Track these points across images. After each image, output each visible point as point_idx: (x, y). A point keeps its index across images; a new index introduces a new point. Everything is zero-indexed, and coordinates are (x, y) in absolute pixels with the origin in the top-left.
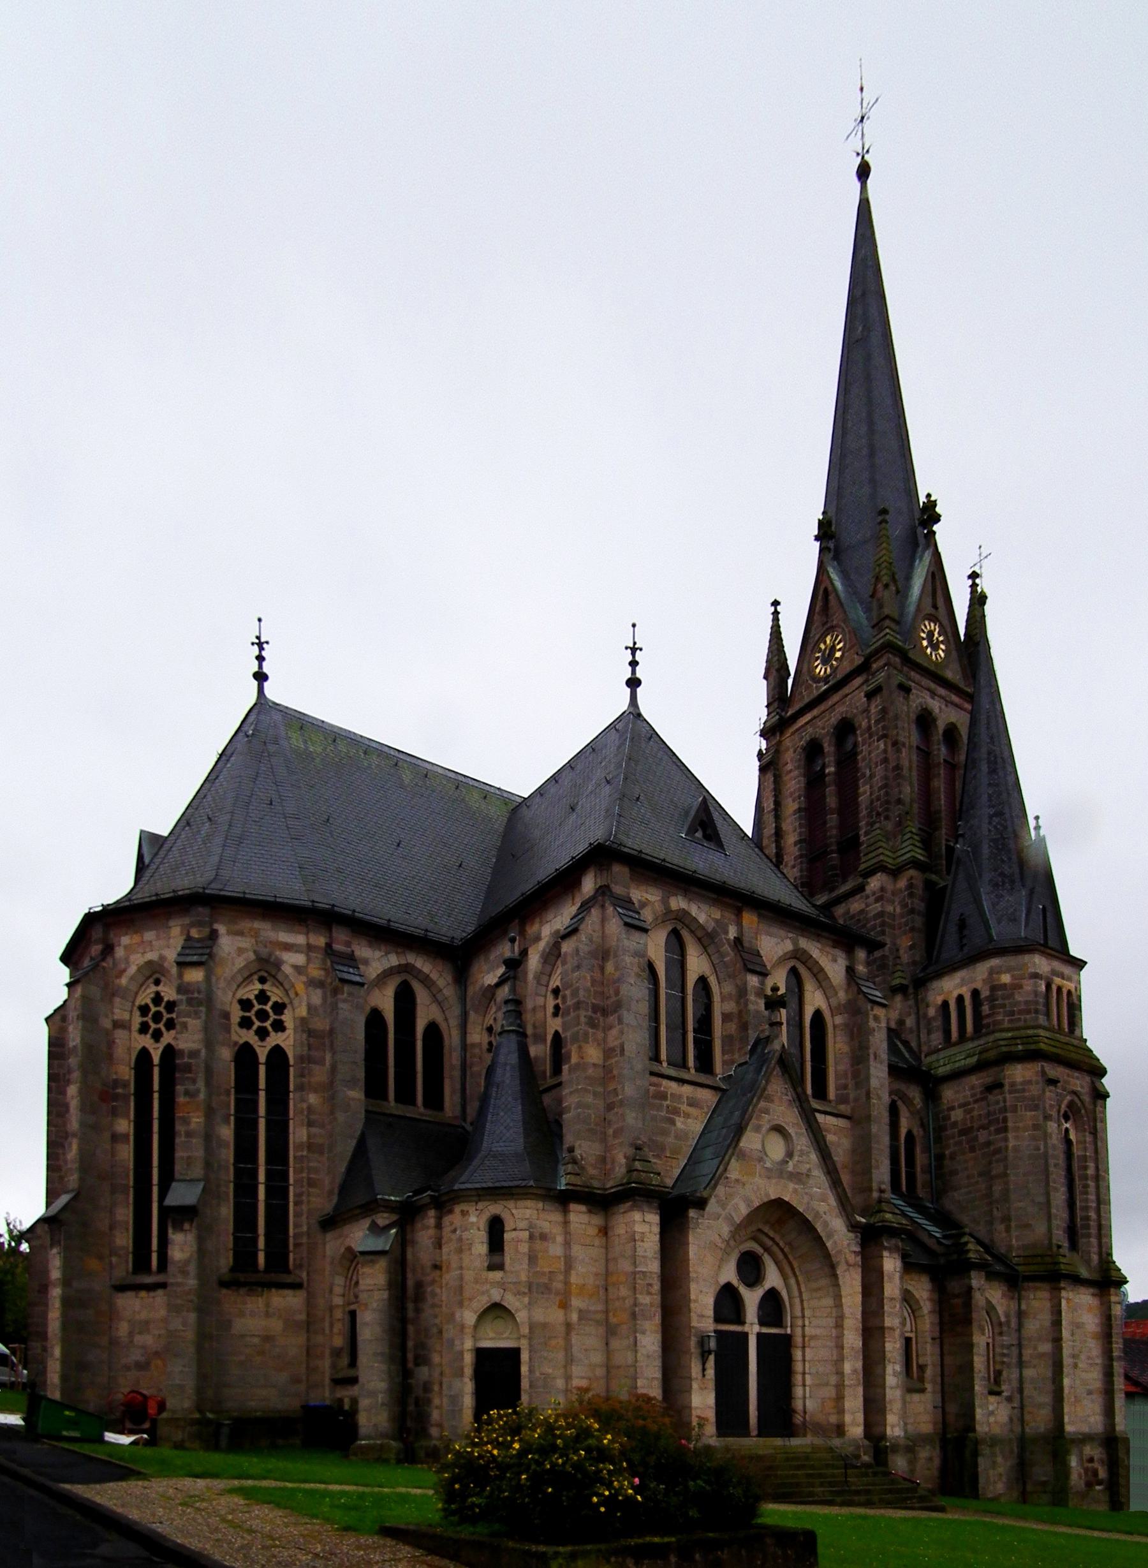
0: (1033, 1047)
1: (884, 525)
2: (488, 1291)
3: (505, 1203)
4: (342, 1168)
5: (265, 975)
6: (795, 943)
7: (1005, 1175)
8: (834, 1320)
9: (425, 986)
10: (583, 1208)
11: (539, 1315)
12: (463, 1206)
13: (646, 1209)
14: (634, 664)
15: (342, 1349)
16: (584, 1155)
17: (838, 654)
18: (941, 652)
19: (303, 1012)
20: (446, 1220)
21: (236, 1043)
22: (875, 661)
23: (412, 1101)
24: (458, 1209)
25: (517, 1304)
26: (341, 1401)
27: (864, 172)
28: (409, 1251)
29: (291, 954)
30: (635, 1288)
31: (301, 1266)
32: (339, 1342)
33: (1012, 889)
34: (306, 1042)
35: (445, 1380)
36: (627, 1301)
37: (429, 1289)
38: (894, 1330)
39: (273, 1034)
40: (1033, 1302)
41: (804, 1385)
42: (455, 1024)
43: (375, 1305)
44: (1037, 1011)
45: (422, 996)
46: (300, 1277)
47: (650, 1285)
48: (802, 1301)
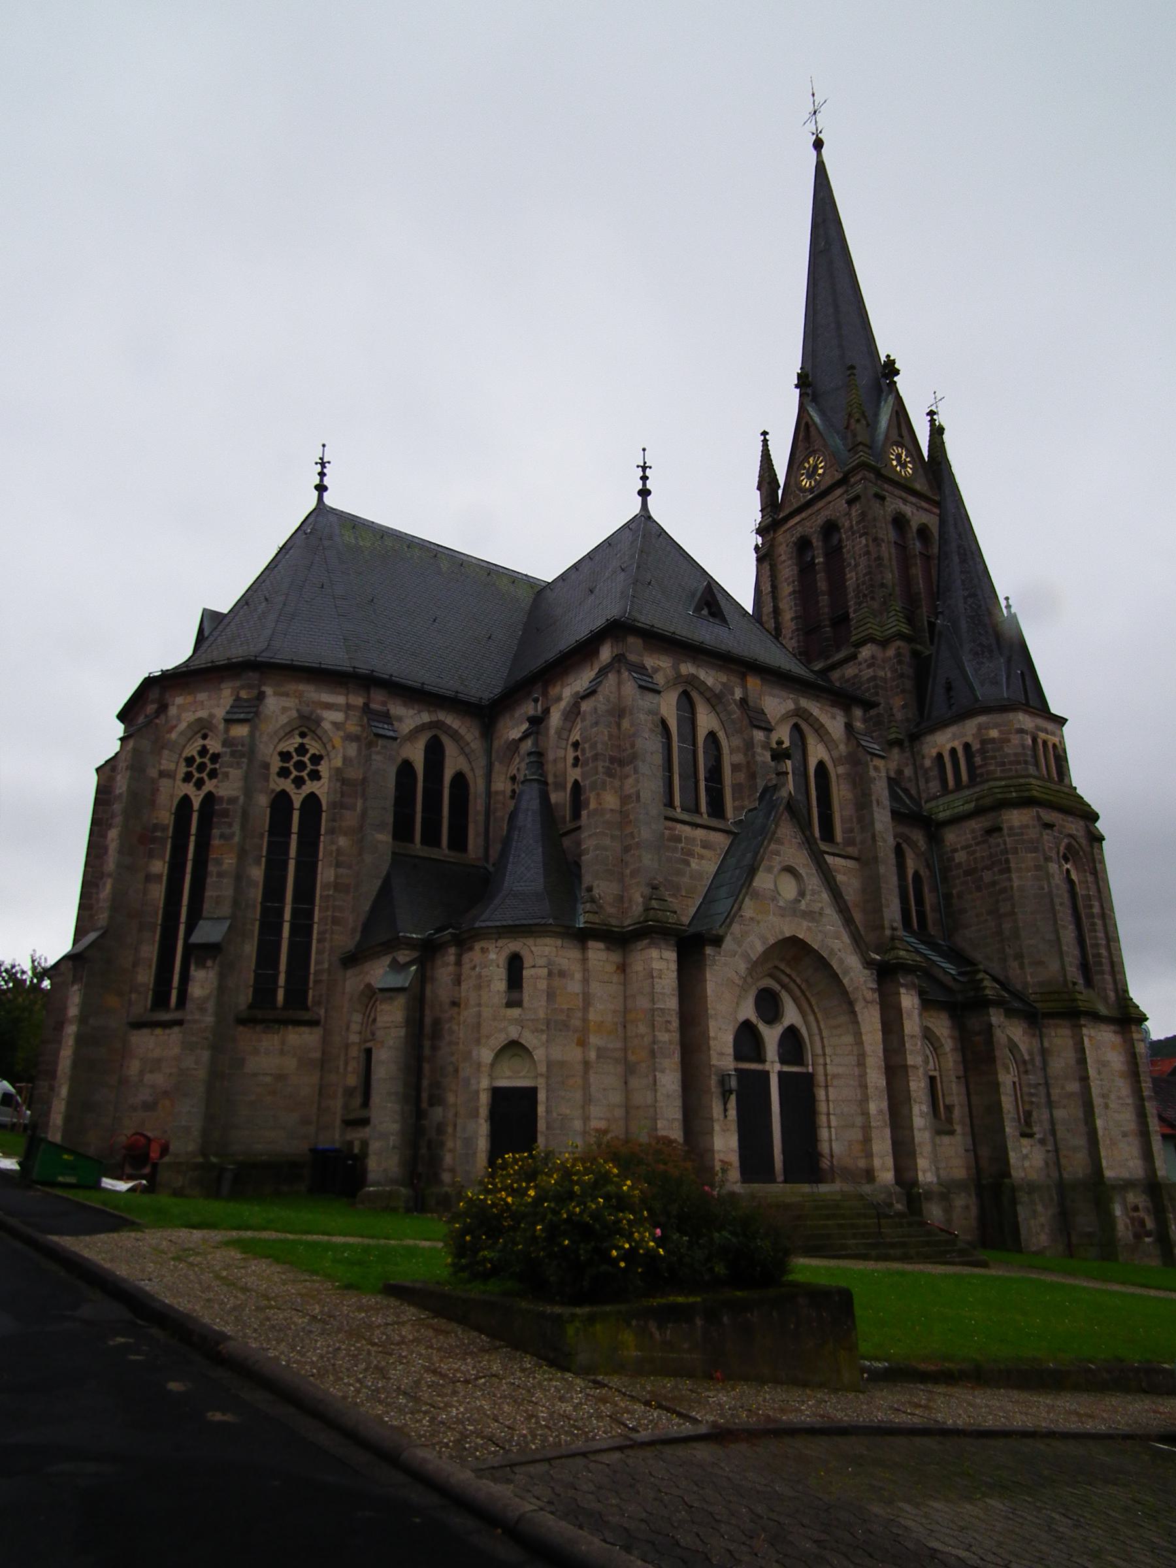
0: (1026, 794)
1: (852, 377)
4: (366, 906)
5: (306, 730)
6: (796, 703)
8: (855, 1058)
9: (454, 740)
10: (601, 945)
11: (557, 1054)
12: (483, 944)
14: (644, 478)
16: (602, 895)
17: (820, 471)
18: (909, 470)
19: (338, 763)
21: (273, 791)
22: (853, 476)
23: (438, 844)
24: (477, 946)
26: (350, 1144)
27: (818, 144)
30: (653, 1024)
32: (352, 1080)
35: (459, 1121)
36: (645, 1039)
37: (447, 1026)
39: (308, 782)
41: (829, 1127)
43: (391, 1043)
44: (1026, 762)
45: (450, 748)
47: (669, 1022)
48: (822, 1039)
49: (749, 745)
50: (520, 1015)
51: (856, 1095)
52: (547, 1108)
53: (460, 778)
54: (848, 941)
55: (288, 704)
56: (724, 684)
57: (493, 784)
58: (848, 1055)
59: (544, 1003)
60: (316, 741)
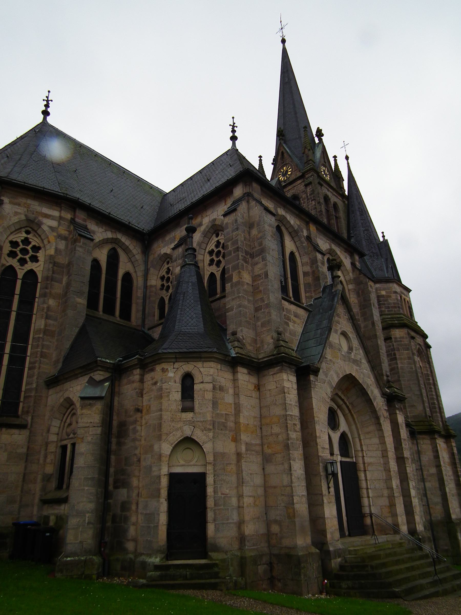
0: (402, 322)
1: (306, 131)
2: (181, 428)
3: (195, 364)
4: (67, 345)
5: (30, 229)
6: (330, 246)
7: (399, 381)
8: (381, 452)
9: (125, 252)
10: (245, 371)
11: (220, 448)
12: (164, 366)
13: (289, 372)
15: (52, 475)
16: (245, 337)
19: (52, 252)
20: (148, 377)
21: (3, 265)
22: (307, 174)
23: (113, 314)
24: (158, 368)
25: (204, 437)
26: (47, 518)
27: (283, 41)
28: (116, 399)
29: (48, 220)
30: (287, 426)
31: (28, 412)
32: (50, 469)
33: (378, 258)
34: (51, 269)
35: (141, 500)
36: (280, 436)
37: (131, 427)
38: (408, 459)
39: (29, 263)
40: (423, 446)
41: (368, 497)
42: (141, 274)
43: (89, 439)
44: (399, 307)
45: (123, 257)
46: (27, 421)
47: (295, 424)
48: (360, 440)
49: (314, 262)
50: (192, 418)
51: (383, 477)
52: (214, 488)
53: (127, 276)
54: (373, 380)
55: (19, 211)
56: (298, 226)
57: (148, 281)
58: (376, 450)
59: (210, 409)
60: (37, 237)
